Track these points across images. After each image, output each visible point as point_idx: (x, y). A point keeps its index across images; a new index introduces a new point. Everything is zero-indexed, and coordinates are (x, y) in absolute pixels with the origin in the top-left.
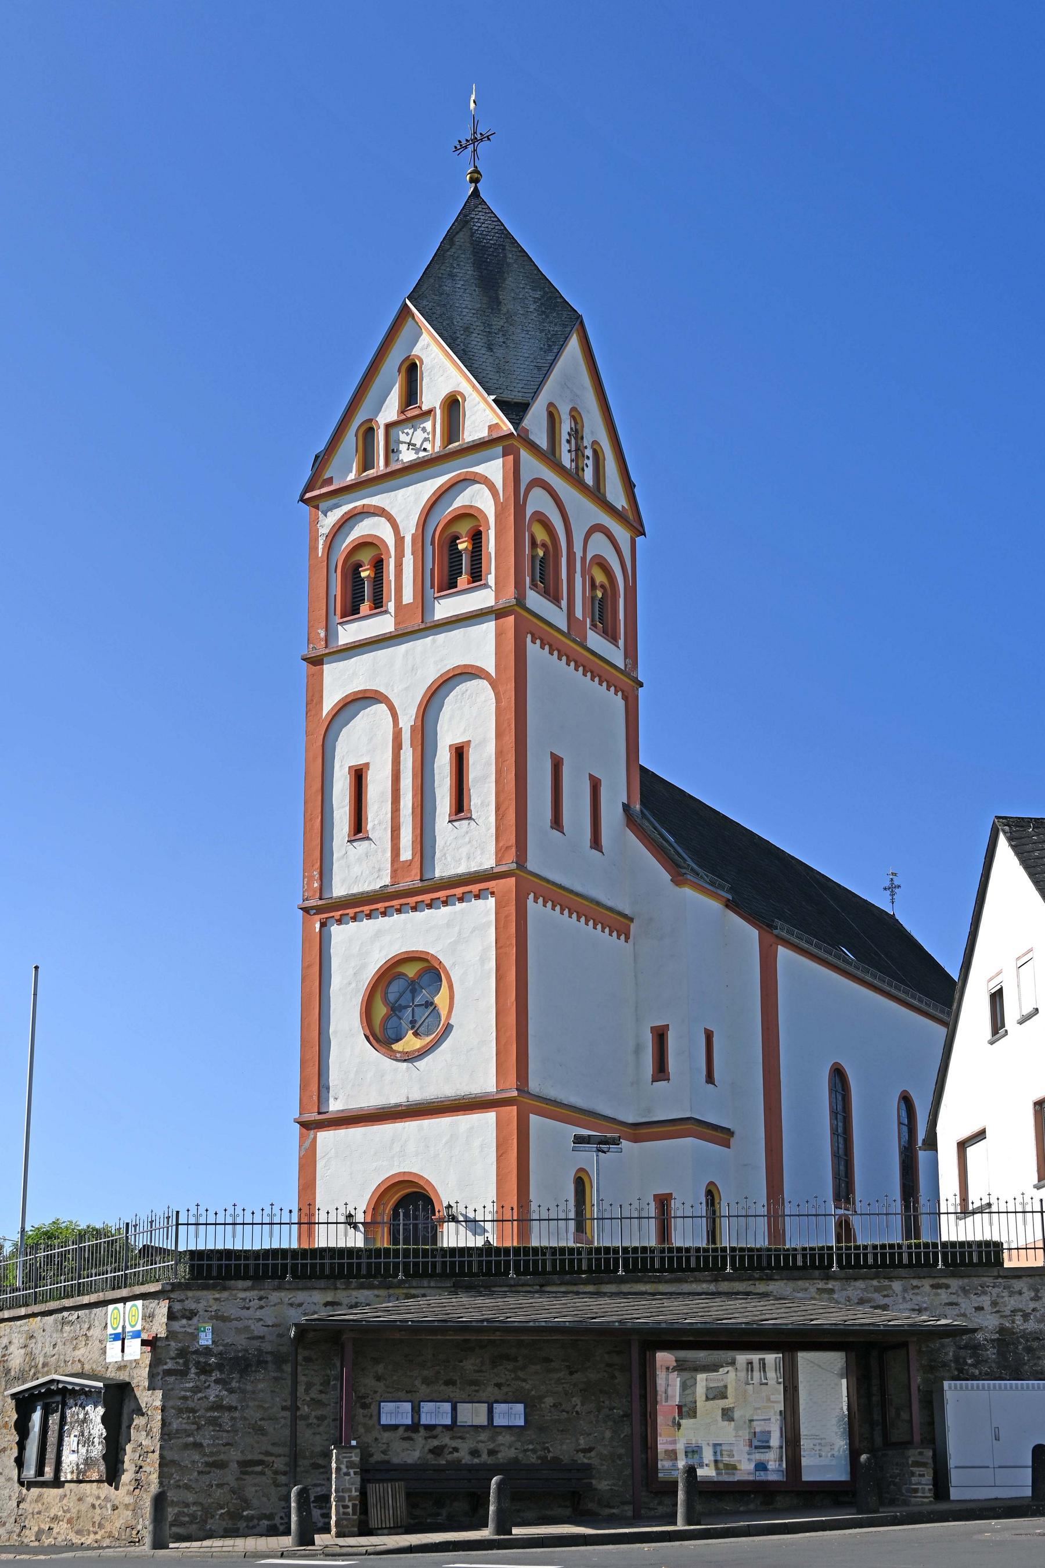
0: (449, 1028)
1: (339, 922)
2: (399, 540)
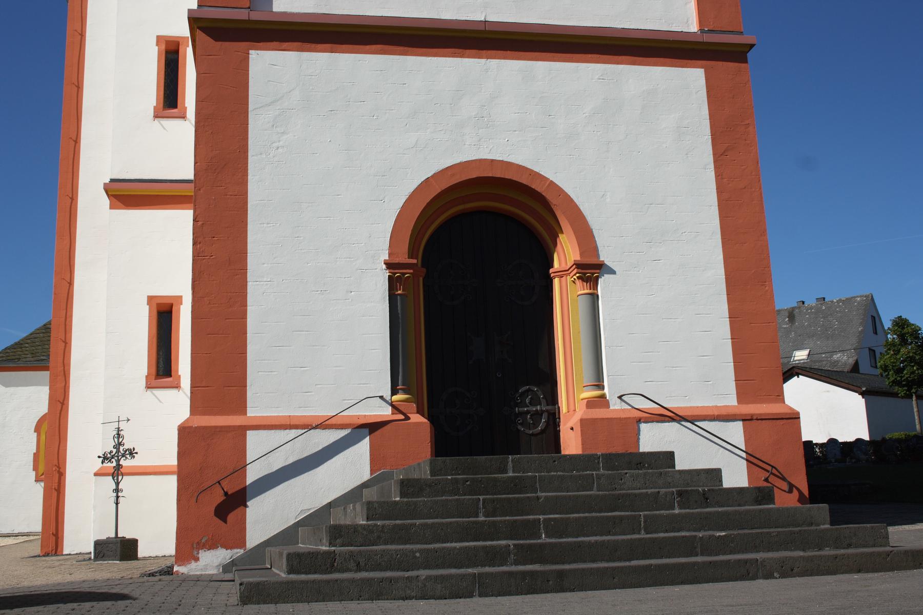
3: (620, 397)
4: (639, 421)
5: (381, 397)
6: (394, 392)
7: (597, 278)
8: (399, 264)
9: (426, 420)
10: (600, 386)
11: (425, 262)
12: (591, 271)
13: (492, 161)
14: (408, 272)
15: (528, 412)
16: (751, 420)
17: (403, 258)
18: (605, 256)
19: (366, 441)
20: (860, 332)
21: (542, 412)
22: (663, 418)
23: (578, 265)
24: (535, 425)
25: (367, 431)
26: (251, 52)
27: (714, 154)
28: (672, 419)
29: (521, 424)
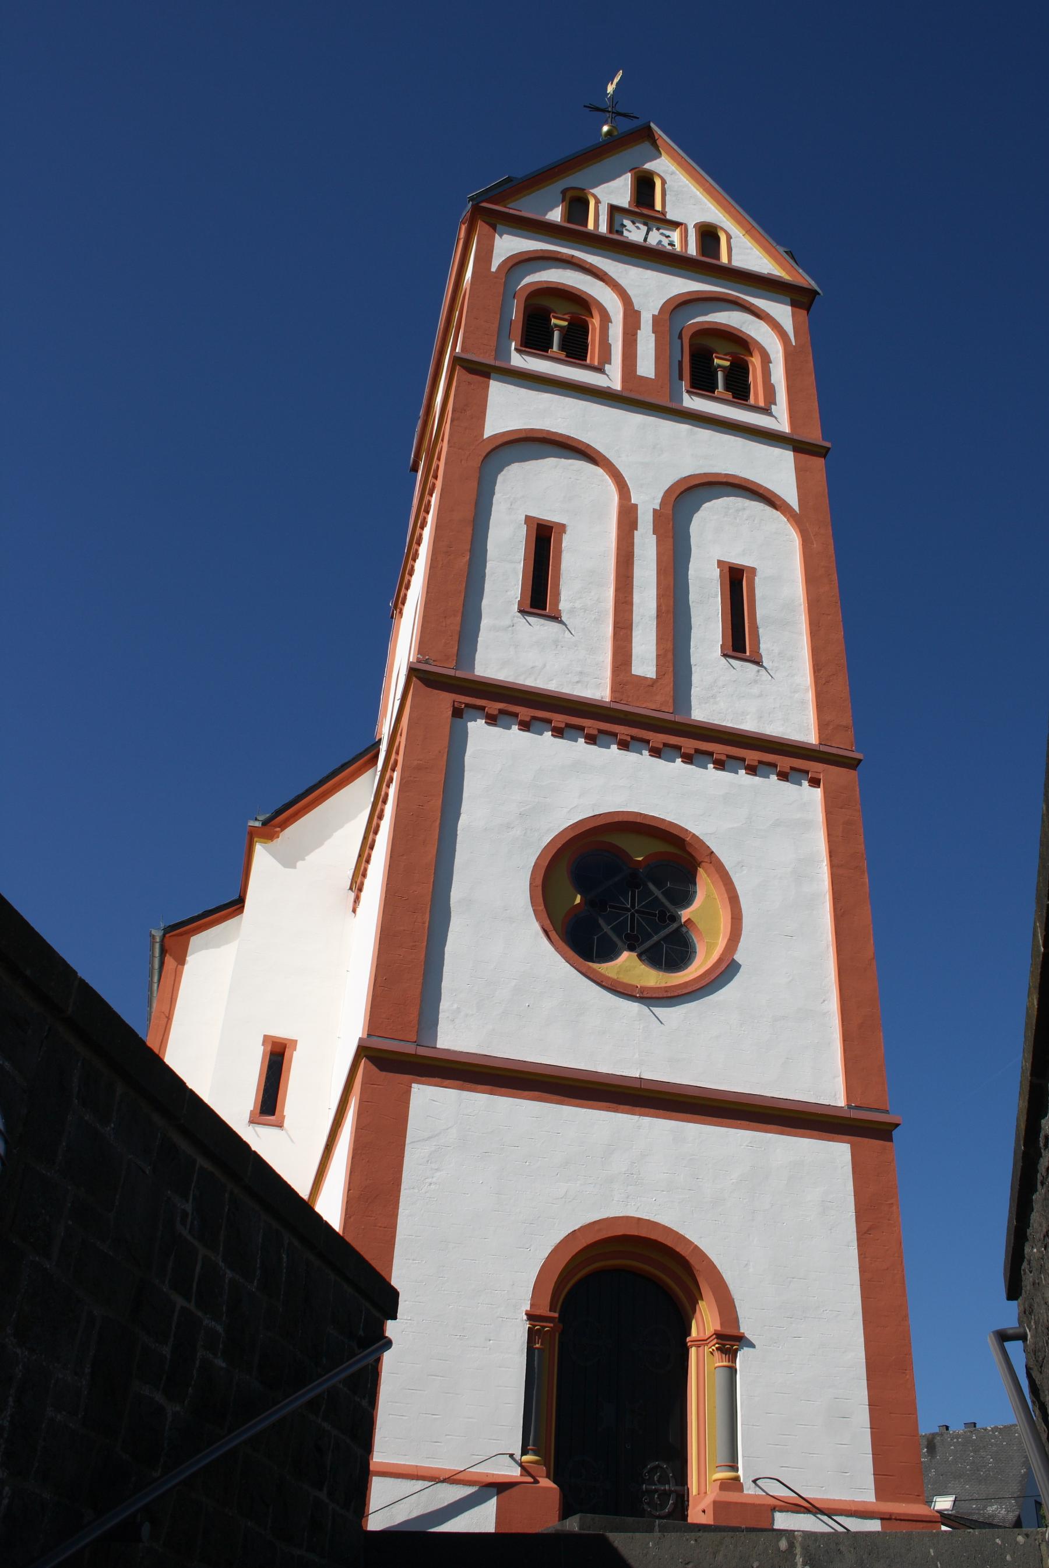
0: (726, 970)
1: (492, 720)
2: (632, 318)
3: (754, 1481)
4: (774, 1509)
5: (511, 1456)
6: (524, 1452)
7: (736, 1352)
8: (540, 1316)
9: (555, 1486)
10: (734, 1468)
11: (561, 1318)
12: (730, 1342)
13: (639, 1219)
14: (548, 1326)
15: (656, 1491)
16: (890, 1519)
17: (544, 1310)
18: (746, 1328)
19: (493, 1502)
20: (1023, 1476)
21: (671, 1492)
22: (798, 1508)
23: (719, 1336)
24: (663, 1506)
25: (495, 1490)
26: (414, 1085)
27: (858, 1232)
28: (807, 1511)
29: (648, 1504)
